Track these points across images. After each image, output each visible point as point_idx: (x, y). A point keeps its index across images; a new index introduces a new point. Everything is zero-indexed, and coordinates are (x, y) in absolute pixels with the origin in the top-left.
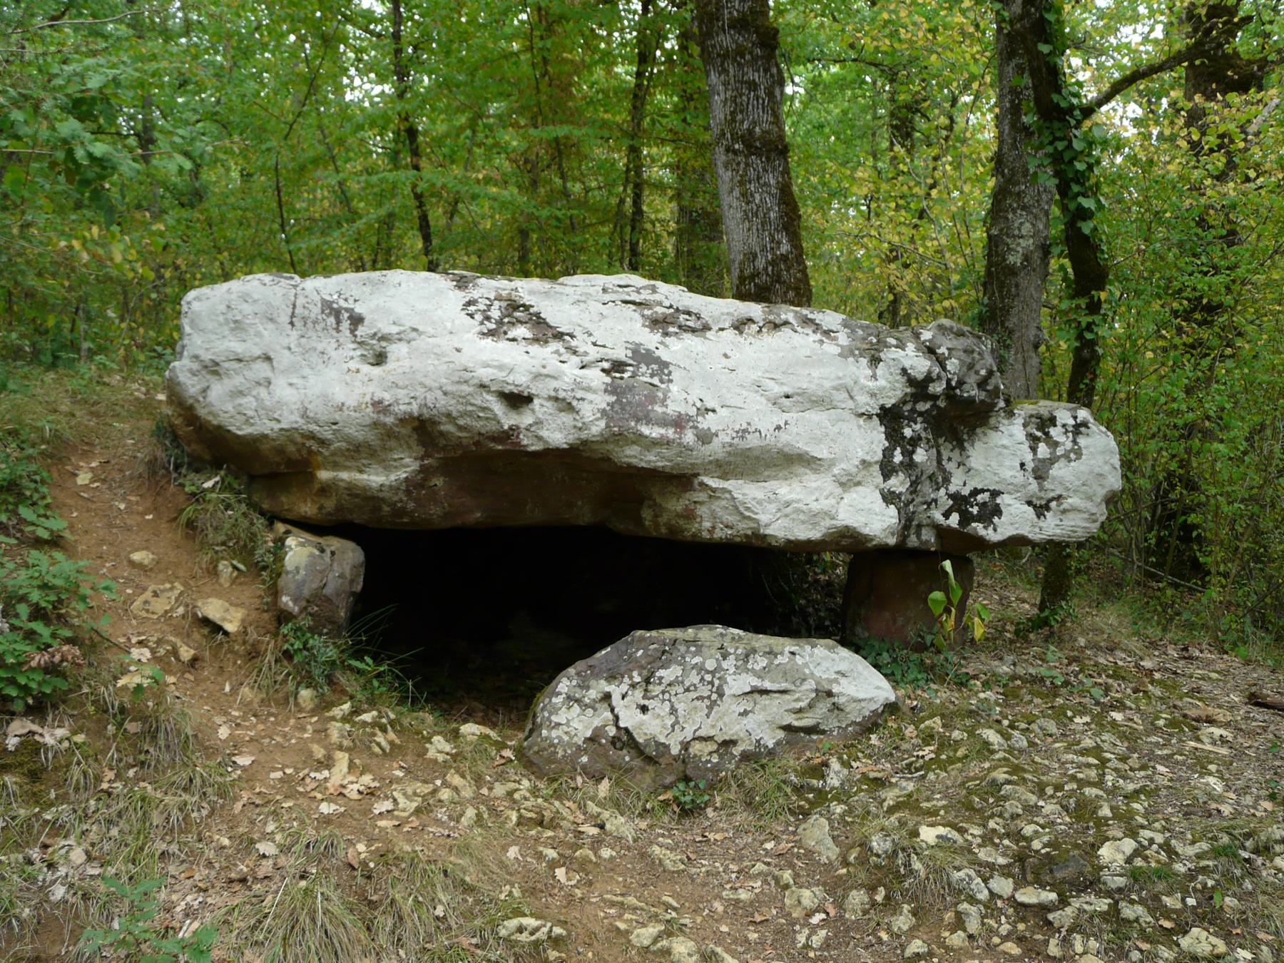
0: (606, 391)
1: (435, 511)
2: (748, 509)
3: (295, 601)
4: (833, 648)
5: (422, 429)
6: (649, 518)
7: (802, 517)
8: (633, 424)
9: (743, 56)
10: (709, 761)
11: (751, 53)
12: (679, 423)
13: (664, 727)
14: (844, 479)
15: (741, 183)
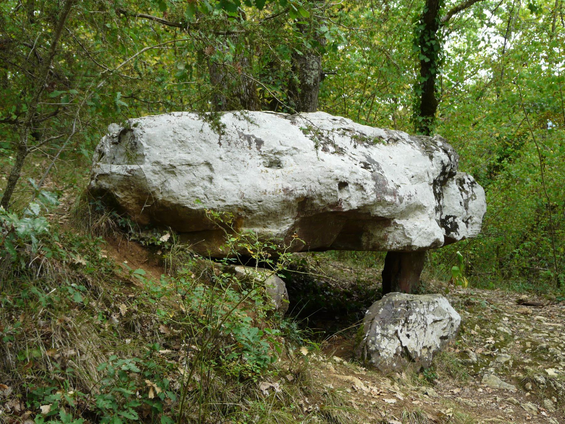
5: (304, 204)
6: (365, 241)
7: (425, 236)
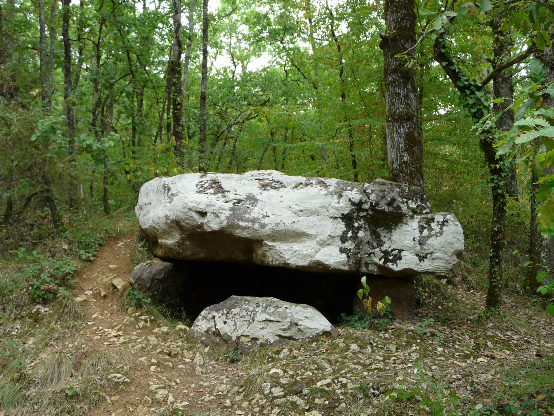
1: (189, 253)
2: (281, 253)
3: (133, 279)
4: (306, 307)
5: (177, 224)
7: (300, 256)
9: (395, 83)
10: (246, 345)
11: (398, 82)
12: (253, 221)
13: (231, 330)
14: (321, 243)
15: (391, 134)
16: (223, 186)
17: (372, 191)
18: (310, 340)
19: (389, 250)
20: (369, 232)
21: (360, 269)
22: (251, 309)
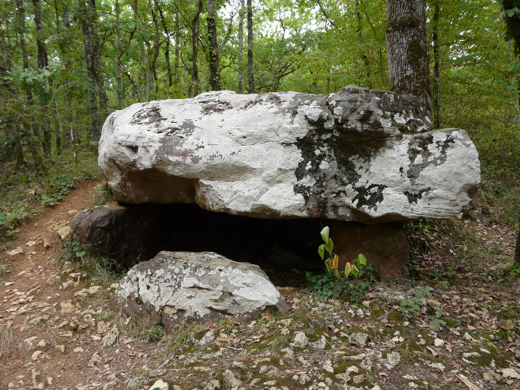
0: (160, 142)
1: (132, 196)
2: (219, 195)
7: (241, 199)
8: (166, 156)
10: (172, 318)
12: (184, 154)
14: (268, 179)
15: (391, 45)
16: (162, 113)
17: (338, 102)
18: (250, 316)
19: (367, 187)
20: (335, 162)
21: (326, 214)
22: (177, 271)
